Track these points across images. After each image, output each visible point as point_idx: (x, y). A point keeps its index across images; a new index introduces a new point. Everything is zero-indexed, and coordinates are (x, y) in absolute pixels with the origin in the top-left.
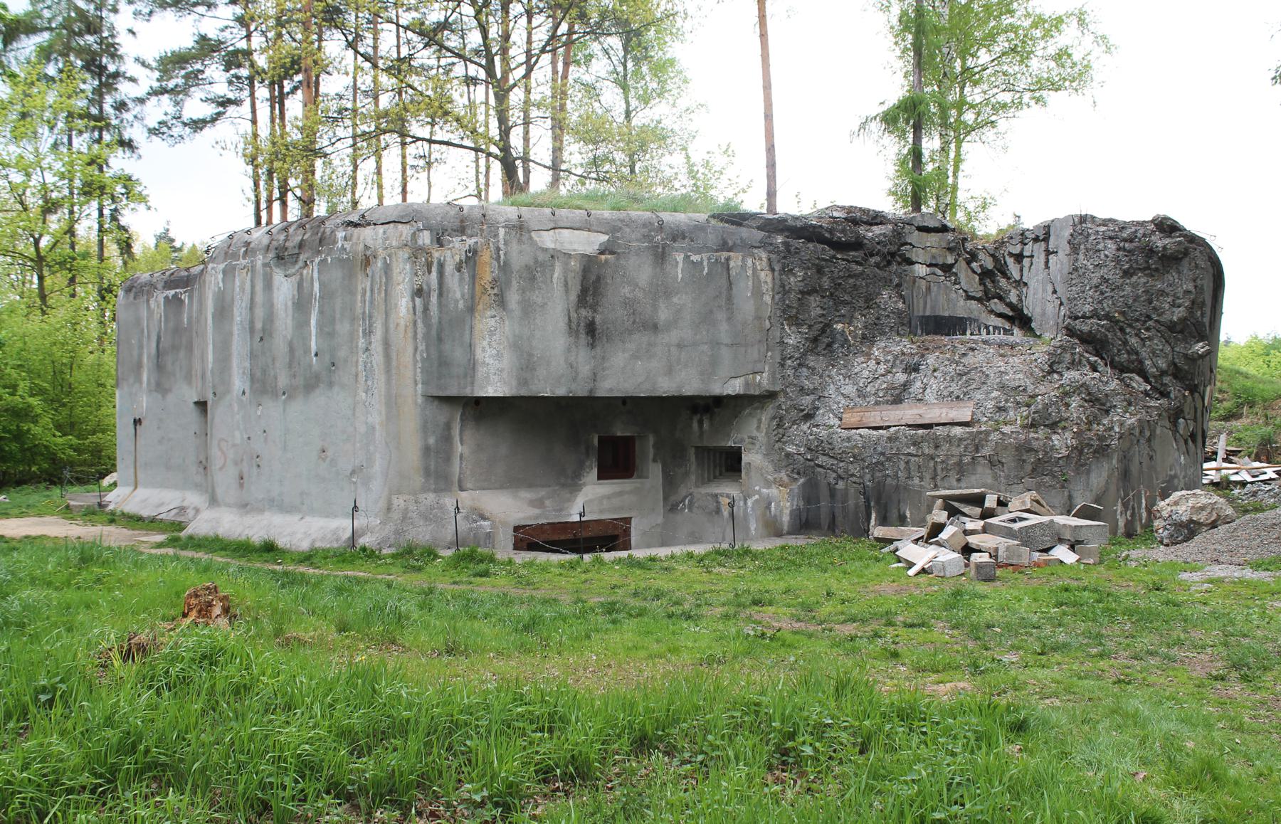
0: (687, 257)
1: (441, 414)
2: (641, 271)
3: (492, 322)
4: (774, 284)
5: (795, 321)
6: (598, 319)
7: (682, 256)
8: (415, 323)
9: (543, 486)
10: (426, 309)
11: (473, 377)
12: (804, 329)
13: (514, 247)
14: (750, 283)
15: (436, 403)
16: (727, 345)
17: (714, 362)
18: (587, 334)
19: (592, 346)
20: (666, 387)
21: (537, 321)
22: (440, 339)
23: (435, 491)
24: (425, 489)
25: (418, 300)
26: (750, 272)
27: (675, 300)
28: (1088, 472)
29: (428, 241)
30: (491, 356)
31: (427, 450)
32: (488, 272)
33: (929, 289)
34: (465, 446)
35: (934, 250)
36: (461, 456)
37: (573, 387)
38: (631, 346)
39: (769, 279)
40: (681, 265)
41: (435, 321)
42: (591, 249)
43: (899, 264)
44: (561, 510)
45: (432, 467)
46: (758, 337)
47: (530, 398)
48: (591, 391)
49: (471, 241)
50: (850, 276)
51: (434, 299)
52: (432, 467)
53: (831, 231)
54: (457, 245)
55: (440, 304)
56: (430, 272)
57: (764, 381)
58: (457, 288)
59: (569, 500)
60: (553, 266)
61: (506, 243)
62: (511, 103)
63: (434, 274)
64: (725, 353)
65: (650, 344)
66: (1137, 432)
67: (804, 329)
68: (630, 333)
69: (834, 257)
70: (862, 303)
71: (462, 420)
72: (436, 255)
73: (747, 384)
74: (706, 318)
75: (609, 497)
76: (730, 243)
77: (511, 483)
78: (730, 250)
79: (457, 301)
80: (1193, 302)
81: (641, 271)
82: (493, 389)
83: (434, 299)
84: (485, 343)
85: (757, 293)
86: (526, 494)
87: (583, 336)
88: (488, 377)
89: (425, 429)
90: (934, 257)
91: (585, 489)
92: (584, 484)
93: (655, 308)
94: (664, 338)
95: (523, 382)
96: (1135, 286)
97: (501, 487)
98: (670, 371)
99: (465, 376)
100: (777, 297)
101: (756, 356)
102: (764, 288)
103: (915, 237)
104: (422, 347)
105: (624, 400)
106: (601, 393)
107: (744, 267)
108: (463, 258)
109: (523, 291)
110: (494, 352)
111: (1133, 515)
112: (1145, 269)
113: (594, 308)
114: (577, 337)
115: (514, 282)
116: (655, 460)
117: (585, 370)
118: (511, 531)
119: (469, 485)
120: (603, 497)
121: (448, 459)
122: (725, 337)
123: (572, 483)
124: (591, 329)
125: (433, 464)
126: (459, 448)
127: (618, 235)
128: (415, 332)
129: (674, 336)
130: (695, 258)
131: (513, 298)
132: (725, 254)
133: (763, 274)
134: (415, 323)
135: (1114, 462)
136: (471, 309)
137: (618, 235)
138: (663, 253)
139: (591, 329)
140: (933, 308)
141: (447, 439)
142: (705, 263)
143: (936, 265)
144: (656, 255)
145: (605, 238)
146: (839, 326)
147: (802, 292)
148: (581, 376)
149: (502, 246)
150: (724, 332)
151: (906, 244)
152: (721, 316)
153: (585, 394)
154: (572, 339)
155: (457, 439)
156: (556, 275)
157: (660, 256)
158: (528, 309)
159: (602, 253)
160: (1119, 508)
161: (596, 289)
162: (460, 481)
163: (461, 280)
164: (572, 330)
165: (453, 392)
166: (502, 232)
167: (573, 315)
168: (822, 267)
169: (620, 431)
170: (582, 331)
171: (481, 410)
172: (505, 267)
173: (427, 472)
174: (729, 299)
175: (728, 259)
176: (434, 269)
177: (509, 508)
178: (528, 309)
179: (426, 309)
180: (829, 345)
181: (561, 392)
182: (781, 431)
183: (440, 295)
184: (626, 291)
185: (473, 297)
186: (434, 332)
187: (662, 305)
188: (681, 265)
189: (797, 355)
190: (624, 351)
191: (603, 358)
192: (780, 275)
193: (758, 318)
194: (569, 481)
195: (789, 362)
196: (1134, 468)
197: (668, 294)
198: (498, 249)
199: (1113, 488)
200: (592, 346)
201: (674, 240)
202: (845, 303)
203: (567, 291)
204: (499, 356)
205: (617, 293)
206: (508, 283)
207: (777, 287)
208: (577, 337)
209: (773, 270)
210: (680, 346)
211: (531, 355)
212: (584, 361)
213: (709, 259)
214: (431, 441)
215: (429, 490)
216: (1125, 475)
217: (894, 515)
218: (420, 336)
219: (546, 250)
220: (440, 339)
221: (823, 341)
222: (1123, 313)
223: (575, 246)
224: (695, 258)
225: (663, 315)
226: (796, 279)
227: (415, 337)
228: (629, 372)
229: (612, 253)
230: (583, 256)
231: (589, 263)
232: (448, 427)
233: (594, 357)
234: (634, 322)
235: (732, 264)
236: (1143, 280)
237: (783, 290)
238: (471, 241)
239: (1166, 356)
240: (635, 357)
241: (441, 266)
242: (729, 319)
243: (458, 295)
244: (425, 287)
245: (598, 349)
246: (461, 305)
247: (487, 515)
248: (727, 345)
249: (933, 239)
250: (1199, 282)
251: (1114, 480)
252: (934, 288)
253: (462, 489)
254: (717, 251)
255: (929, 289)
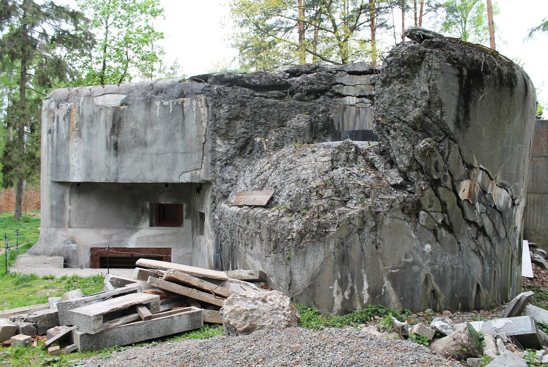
0: (162, 103)
1: (60, 190)
2: (139, 112)
3: (76, 144)
4: (208, 115)
5: (225, 136)
6: (119, 140)
7: (159, 102)
8: (48, 146)
9: (116, 228)
10: (52, 139)
11: (69, 172)
12: (233, 142)
13: (86, 105)
14: (195, 116)
15: (56, 184)
16: (181, 153)
17: (174, 163)
18: (114, 149)
19: (116, 155)
20: (150, 177)
21: (94, 143)
22: (57, 154)
23: (56, 227)
24: (51, 226)
25: (49, 135)
26: (194, 109)
27: (155, 128)
28: (305, 254)
29: (53, 106)
30: (76, 162)
31: (52, 207)
32: (75, 119)
33: (358, 112)
34: (72, 205)
35: (362, 87)
36: (70, 211)
37: (108, 177)
38: (134, 155)
39: (206, 112)
40: (158, 108)
41: (55, 145)
42: (117, 104)
43: (331, 97)
44: (121, 241)
45: (55, 216)
46: (198, 148)
47: (91, 183)
48: (116, 180)
49: (69, 105)
50: (263, 106)
51: (55, 134)
52: (55, 216)
53: (249, 79)
54: (64, 107)
55: (57, 137)
56: (54, 121)
57: (202, 175)
58: (64, 129)
59: (128, 236)
60: (100, 114)
61: (82, 105)
62: (489, 46)
63: (55, 122)
64: (180, 158)
65: (143, 154)
66: (357, 222)
67: (233, 142)
68: (134, 147)
69: (251, 95)
70: (275, 123)
71: (70, 193)
72: (56, 113)
73: (192, 176)
74: (171, 138)
75: (154, 236)
76: (185, 92)
77: (97, 225)
78: (184, 97)
79: (63, 135)
80: (429, 102)
81: (139, 112)
82: (76, 178)
83: (55, 134)
84: (73, 155)
85: (199, 121)
86: (104, 232)
87: (112, 150)
88: (74, 172)
89: (51, 197)
90: (362, 91)
91: (141, 231)
92: (141, 229)
93: (145, 133)
94: (149, 150)
95: (88, 175)
96: (391, 93)
97: (92, 227)
98: (152, 169)
99: (66, 172)
100: (210, 123)
101: (197, 159)
102: (203, 118)
103: (346, 79)
104: (50, 158)
105: (167, 185)
106: (120, 181)
107: (191, 106)
108: (66, 113)
109: (88, 128)
110: (77, 159)
111: (352, 295)
112: (398, 77)
113: (117, 135)
114: (110, 151)
115: (85, 124)
116: (187, 218)
117: (113, 169)
118: (88, 251)
119: (74, 226)
120: (150, 236)
121: (63, 212)
122: (180, 149)
123: (134, 227)
124: (116, 146)
125: (55, 214)
126: (68, 207)
127: (131, 94)
128: (48, 151)
129: (154, 149)
130: (166, 103)
131: (84, 131)
132: (181, 100)
133: (202, 109)
134: (48, 146)
135: (332, 247)
136: (68, 139)
137: (131, 94)
138: (150, 102)
139: (116, 146)
140: (361, 125)
141: (62, 202)
142: (171, 106)
143: (365, 96)
144: (146, 104)
145: (124, 97)
146: (258, 140)
147: (228, 119)
148: (111, 171)
149: (81, 106)
150: (180, 145)
151: (337, 84)
152: (178, 135)
153: (113, 181)
154: (108, 152)
155: (67, 202)
156: (102, 119)
157: (149, 103)
158: (90, 136)
159: (122, 105)
160: (336, 287)
161: (119, 124)
162: (69, 223)
163: (65, 124)
164: (108, 148)
165: (61, 180)
166: (82, 98)
167: (109, 139)
168: (245, 102)
169: (163, 201)
170: (112, 147)
171: (80, 188)
172: (81, 117)
173: (52, 218)
174: (183, 126)
175: (183, 102)
176: (55, 120)
177: (92, 238)
178: (90, 136)
179: (52, 139)
180: (251, 152)
181: (103, 180)
182: (214, 205)
183: (57, 132)
184: (132, 125)
185: (69, 133)
186: (55, 151)
187: (149, 131)
188: (158, 108)
189: (224, 158)
190: (130, 158)
191: (121, 162)
192: (213, 109)
193: (199, 136)
194: (132, 226)
195: (218, 163)
196: (354, 254)
197: (152, 125)
198: (79, 107)
199: (328, 271)
200: (116, 155)
201: (157, 94)
202: (261, 124)
203: (106, 127)
204: (78, 162)
205: (128, 126)
206: (83, 124)
207: (210, 117)
208: (110, 151)
209: (208, 106)
210: (157, 154)
211: (91, 161)
212: (112, 162)
213: (173, 103)
214: (54, 203)
215: (53, 227)
216: (343, 259)
217: (235, 267)
218: (50, 152)
219: (97, 106)
220: (57, 154)
221: (245, 149)
222: (383, 117)
223: (111, 103)
224: (166, 103)
225: (149, 137)
226: (223, 112)
227: (48, 153)
228: (137, 169)
229: (126, 104)
230: (114, 107)
231: (116, 110)
232: (63, 196)
233: (117, 162)
234: (136, 142)
235: (185, 105)
236: (398, 87)
237: (215, 118)
238: (69, 105)
239: (407, 153)
240: (136, 161)
241: (58, 118)
242: (183, 137)
243: (64, 132)
244: (52, 129)
245: (119, 157)
246: (65, 137)
247: (77, 241)
248: (181, 153)
249: (363, 79)
250: (431, 82)
251: (331, 263)
252: (362, 112)
253: (70, 227)
254: (177, 98)
255: (358, 112)
